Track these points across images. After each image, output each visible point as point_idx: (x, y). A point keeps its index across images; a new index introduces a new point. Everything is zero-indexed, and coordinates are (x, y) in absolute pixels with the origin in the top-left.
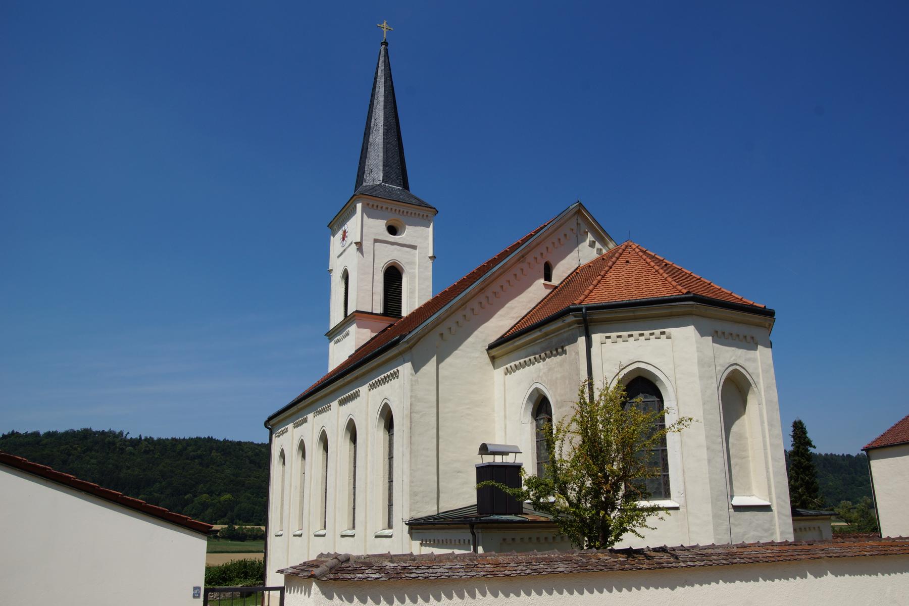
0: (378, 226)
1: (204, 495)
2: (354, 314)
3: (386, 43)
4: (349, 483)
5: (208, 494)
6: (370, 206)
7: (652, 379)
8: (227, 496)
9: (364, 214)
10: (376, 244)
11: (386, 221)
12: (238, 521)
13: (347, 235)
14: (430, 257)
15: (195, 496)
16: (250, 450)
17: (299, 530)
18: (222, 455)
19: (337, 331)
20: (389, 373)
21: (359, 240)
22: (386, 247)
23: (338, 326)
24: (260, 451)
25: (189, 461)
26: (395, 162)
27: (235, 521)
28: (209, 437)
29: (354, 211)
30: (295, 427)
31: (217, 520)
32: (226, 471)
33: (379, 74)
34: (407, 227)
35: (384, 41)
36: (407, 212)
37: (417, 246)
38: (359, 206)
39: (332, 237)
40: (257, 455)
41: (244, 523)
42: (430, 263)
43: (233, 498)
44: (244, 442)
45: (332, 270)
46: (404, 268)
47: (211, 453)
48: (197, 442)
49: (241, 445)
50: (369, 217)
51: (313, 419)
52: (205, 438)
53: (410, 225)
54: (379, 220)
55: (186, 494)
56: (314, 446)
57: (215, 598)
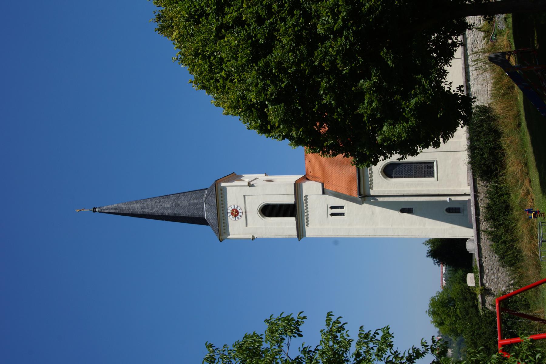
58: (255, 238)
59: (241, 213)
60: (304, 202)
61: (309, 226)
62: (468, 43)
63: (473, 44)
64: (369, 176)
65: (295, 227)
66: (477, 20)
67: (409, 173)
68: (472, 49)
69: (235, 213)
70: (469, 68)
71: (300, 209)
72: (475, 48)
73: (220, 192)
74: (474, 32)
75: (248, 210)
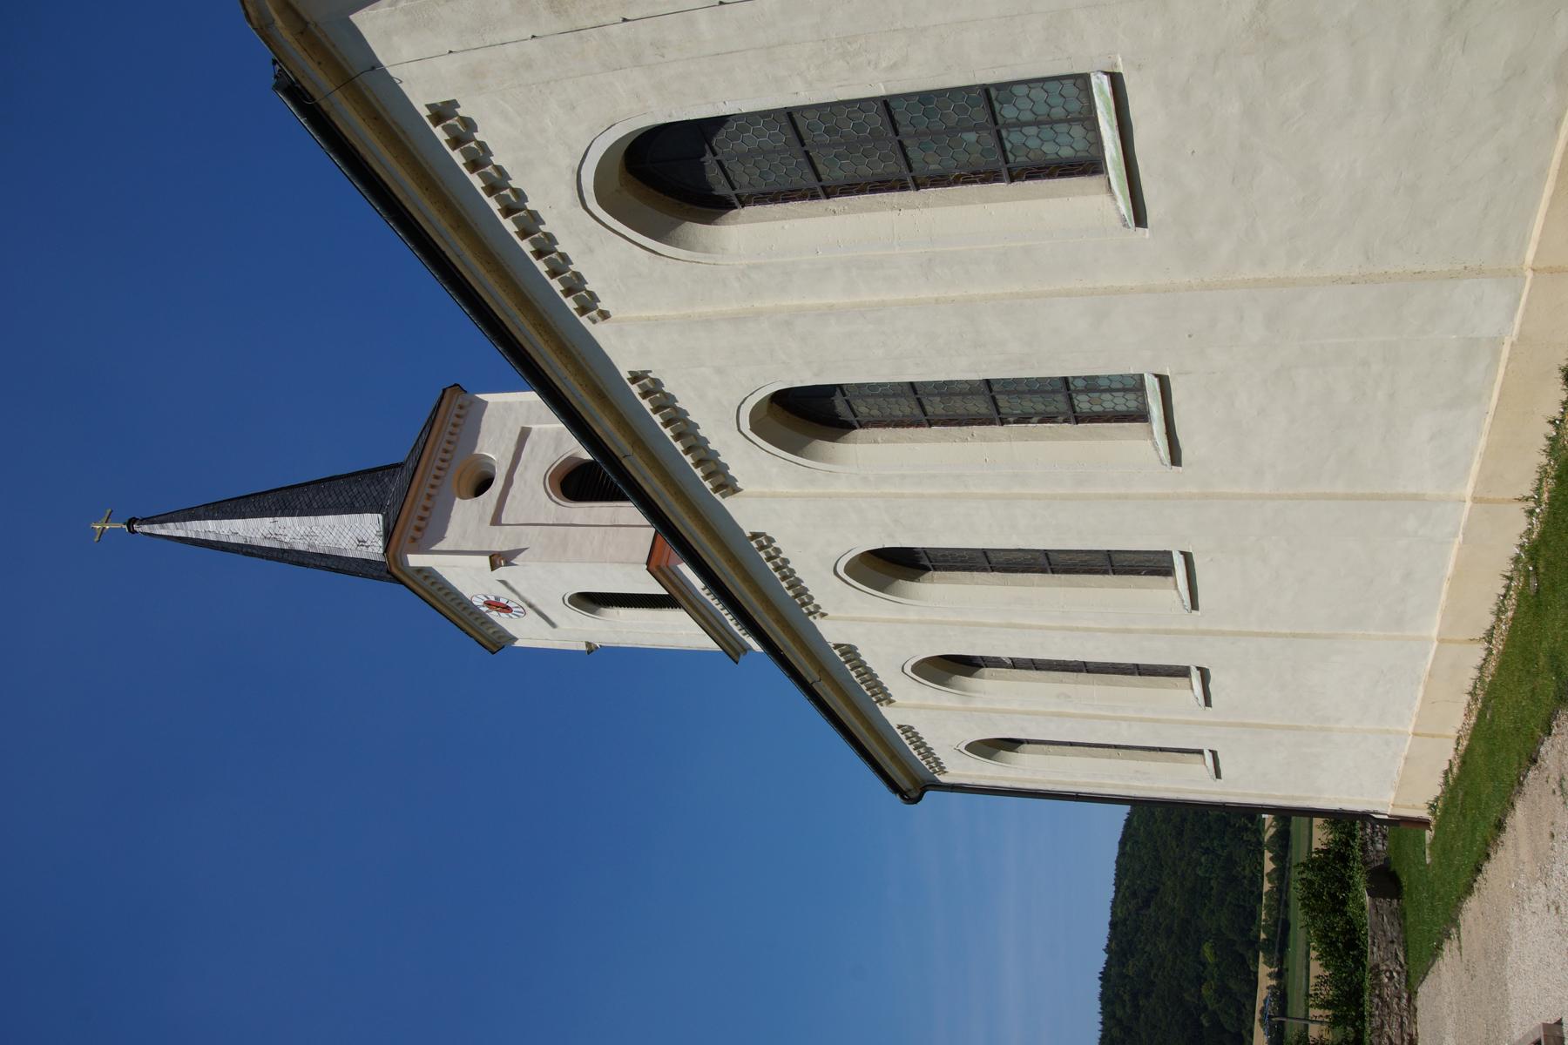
0: (467, 516)
1: (1203, 991)
2: (653, 567)
3: (131, 522)
4: (984, 439)
5: (1203, 984)
6: (418, 535)
8: (1207, 951)
9: (433, 548)
10: (503, 522)
11: (457, 499)
12: (1252, 933)
13: (493, 599)
15: (1205, 1008)
16: (1125, 907)
17: (1192, 688)
18: (1133, 956)
19: (719, 627)
20: (493, 204)
21: (486, 560)
22: (514, 497)
23: (703, 622)
24: (1128, 887)
25: (1143, 1015)
26: (347, 487)
27: (1251, 938)
28: (1100, 978)
29: (427, 573)
30: (890, 701)
31: (1250, 971)
32: (1161, 950)
33: (181, 533)
34: (476, 451)
35: (125, 527)
36: (446, 451)
37: (523, 428)
38: (415, 560)
39: (517, 644)
40: (1134, 894)
41: (1257, 922)
43: (1211, 941)
44: (1111, 916)
45: (588, 644)
46: (568, 455)
47: (1127, 976)
48: (1109, 1000)
49: (1117, 922)
50: (441, 537)
51: (833, 619)
52: (1102, 986)
53: (474, 445)
54: (452, 514)
55: (1202, 1026)
56: (912, 615)
57: (1401, 966)
75: (533, 601)
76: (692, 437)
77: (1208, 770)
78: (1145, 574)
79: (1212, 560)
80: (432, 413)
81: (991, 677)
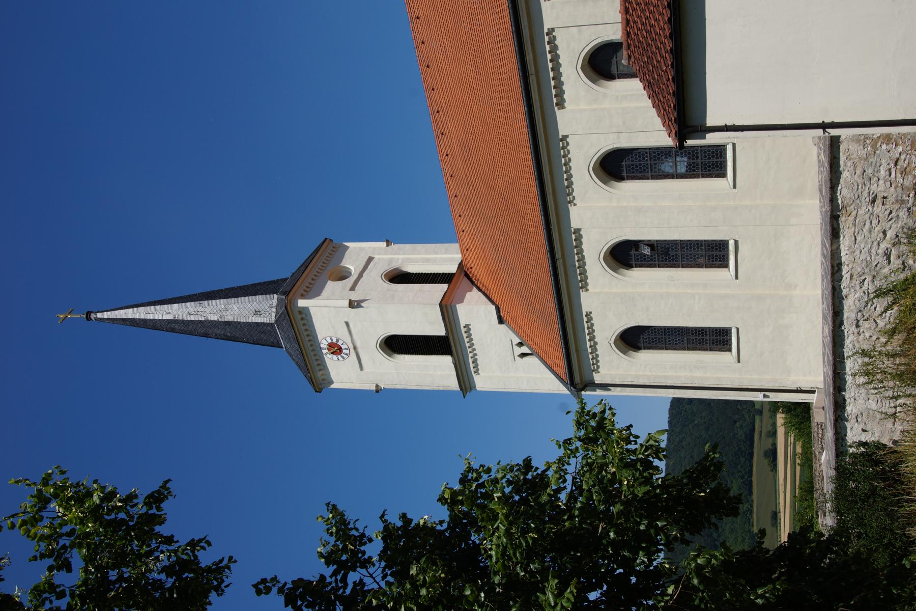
7: (611, 42)
14: (387, 245)
37: (370, 257)
42: (394, 247)
54: (326, 287)
58: (381, 389)
59: (346, 349)
60: (465, 335)
61: (479, 372)
62: (845, 307)
63: (860, 311)
64: (590, 350)
65: (454, 373)
66: (877, 254)
67: (676, 341)
68: (858, 321)
69: (335, 349)
70: (844, 363)
71: (458, 348)
72: (867, 319)
73: (299, 317)
74: (866, 283)
75: (358, 345)
76: (557, 72)
77: (734, 358)
78: (715, 177)
79: (743, 148)
80: (314, 252)
81: (637, 271)
